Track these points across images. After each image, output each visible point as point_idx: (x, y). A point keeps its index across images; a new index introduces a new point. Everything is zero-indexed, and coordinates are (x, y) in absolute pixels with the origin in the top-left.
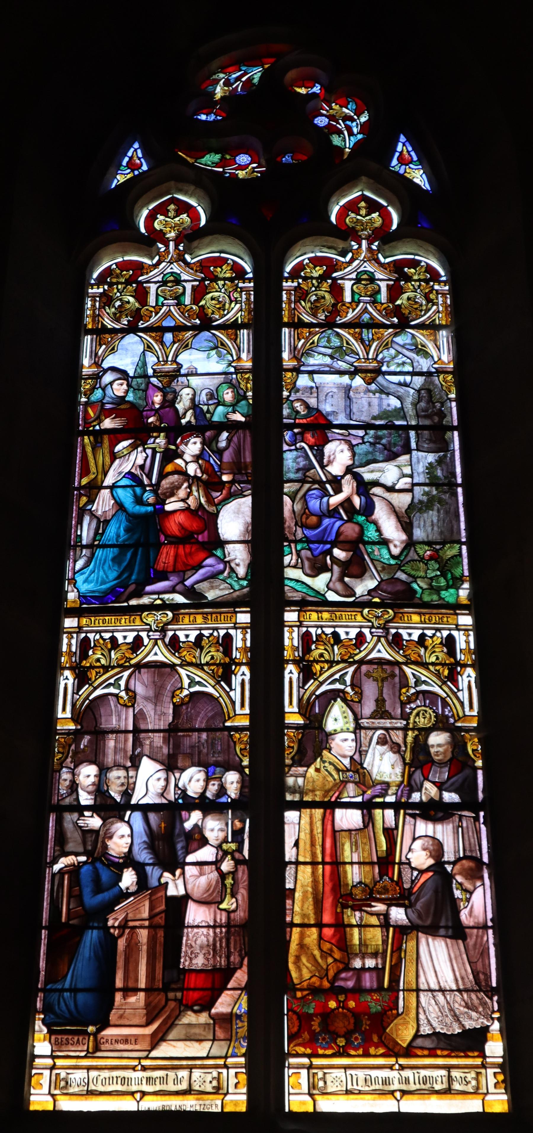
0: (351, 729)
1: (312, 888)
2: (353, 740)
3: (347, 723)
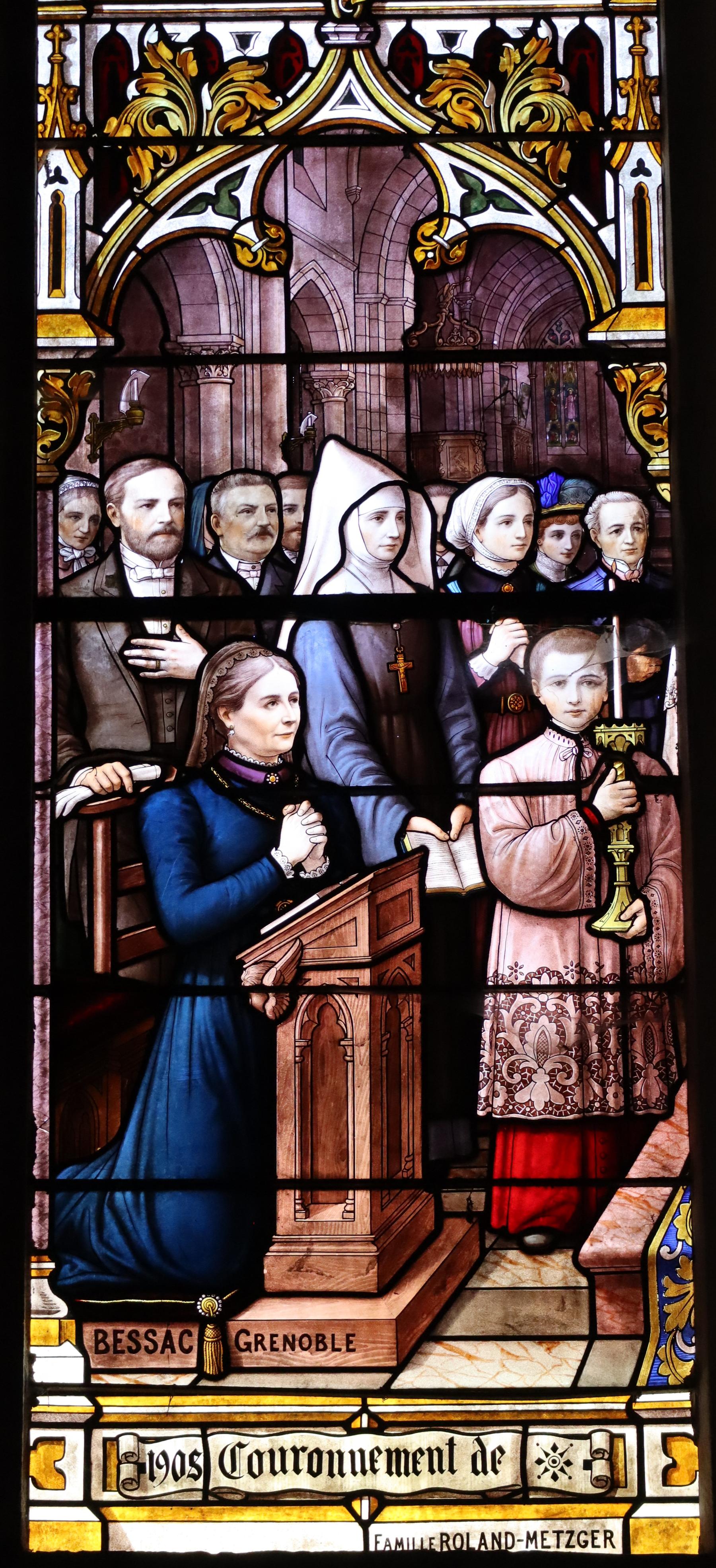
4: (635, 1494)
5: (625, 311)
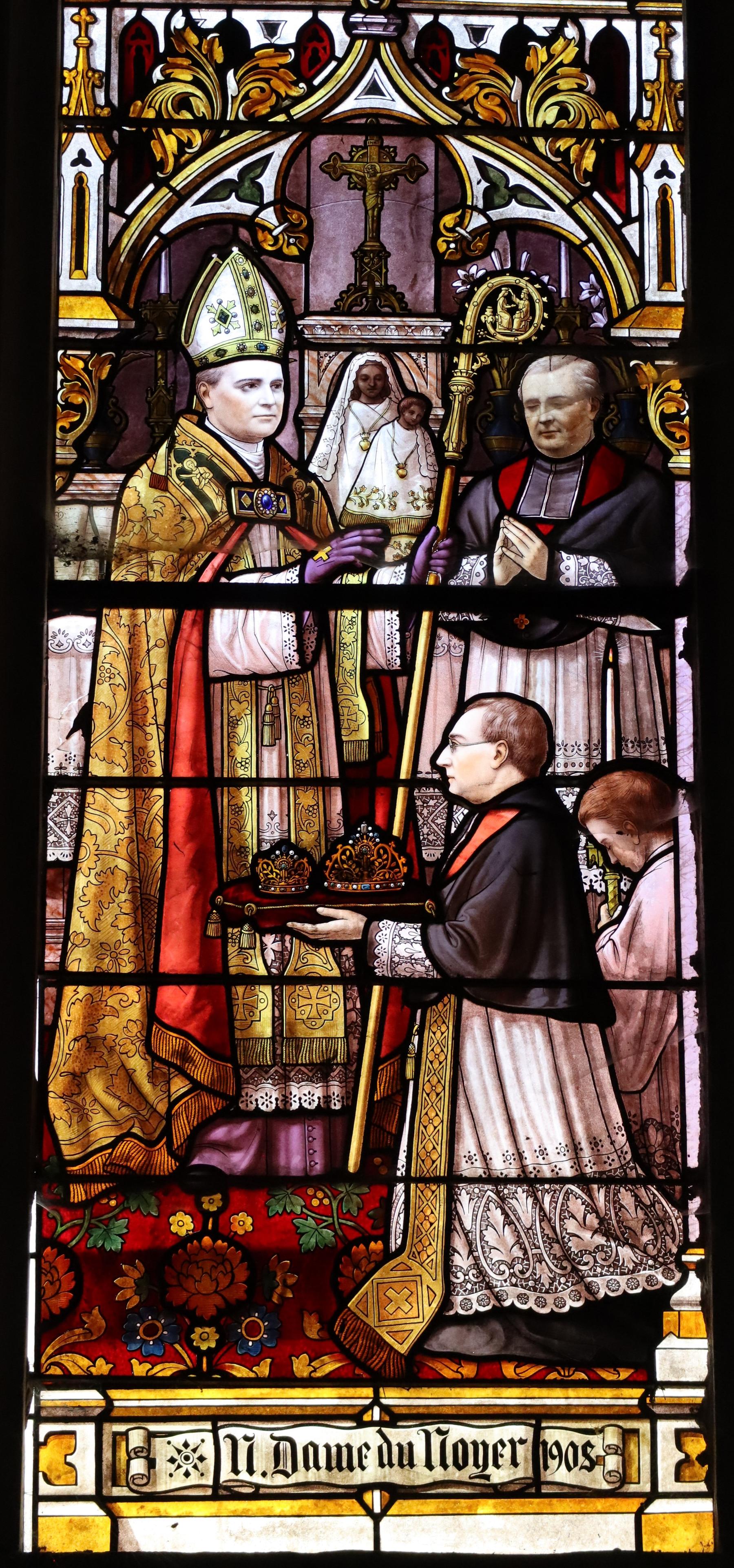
0: (273, 349)
1: (131, 862)
2: (275, 385)
4: (647, 1488)
5: (647, 310)
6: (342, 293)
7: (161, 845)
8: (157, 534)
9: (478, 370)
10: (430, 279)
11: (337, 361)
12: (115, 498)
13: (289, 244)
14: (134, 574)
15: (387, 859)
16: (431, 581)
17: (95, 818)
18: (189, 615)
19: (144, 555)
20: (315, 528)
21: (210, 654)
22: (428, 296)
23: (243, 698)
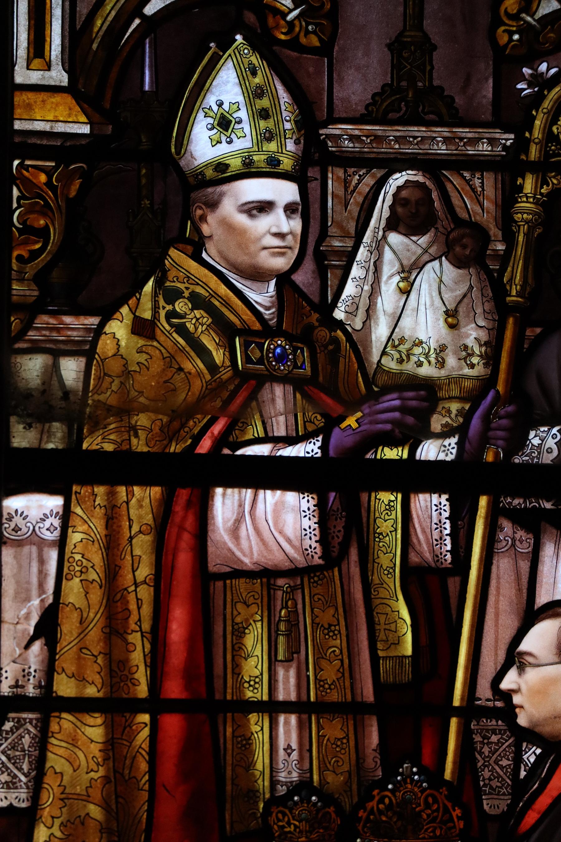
0: (287, 164)
1: (105, 806)
2: (290, 209)
3: (269, 136)
6: (374, 95)
7: (147, 787)
8: (141, 393)
9: (548, 195)
10: (487, 79)
11: (369, 181)
12: (87, 347)
13: (307, 33)
14: (113, 442)
15: (437, 810)
16: (489, 457)
17: (61, 751)
18: (183, 495)
19: (125, 418)
20: (341, 389)
21: (209, 543)
22: (484, 101)
23: (251, 600)
